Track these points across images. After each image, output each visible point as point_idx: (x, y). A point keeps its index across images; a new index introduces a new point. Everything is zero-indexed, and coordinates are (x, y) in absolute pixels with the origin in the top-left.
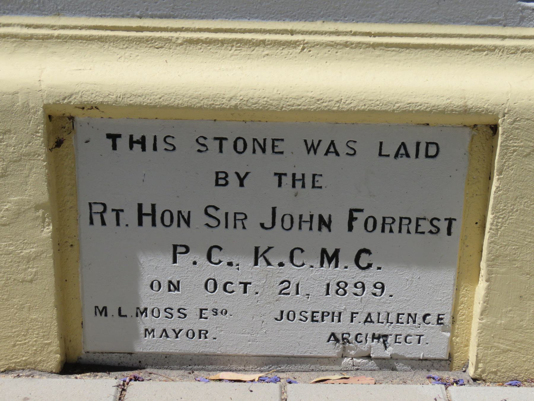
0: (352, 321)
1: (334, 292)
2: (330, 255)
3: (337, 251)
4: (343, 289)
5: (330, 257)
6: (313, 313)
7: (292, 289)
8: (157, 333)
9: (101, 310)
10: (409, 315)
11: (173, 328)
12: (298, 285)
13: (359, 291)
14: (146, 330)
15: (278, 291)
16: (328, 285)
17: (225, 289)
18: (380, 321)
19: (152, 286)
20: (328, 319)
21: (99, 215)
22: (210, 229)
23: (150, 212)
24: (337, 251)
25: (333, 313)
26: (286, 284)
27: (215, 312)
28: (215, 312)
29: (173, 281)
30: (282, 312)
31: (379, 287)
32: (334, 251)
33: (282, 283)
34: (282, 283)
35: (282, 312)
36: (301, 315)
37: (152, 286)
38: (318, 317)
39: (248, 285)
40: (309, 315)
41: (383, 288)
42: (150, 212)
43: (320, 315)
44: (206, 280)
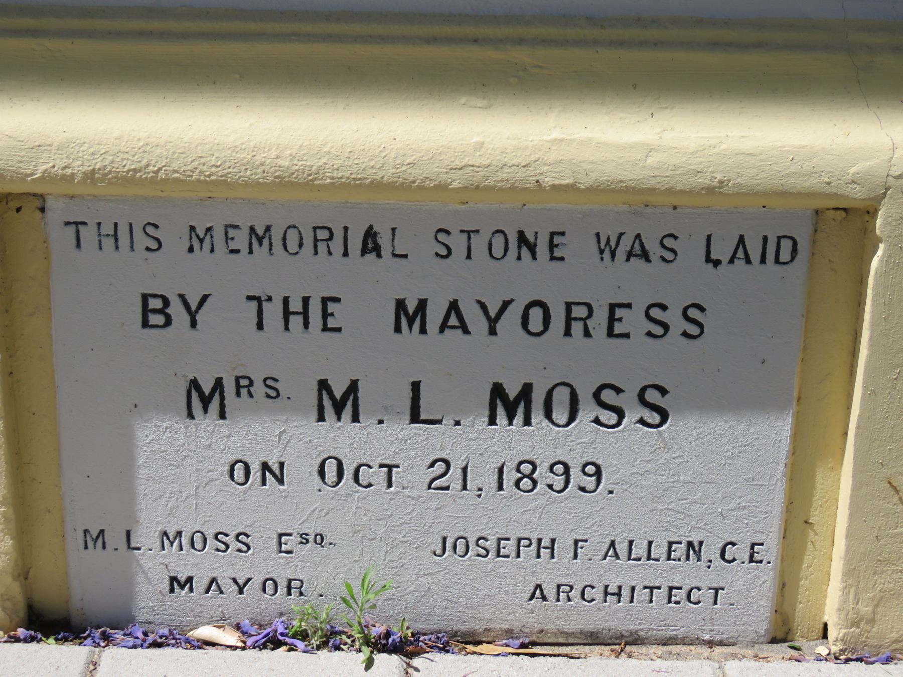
0: (576, 556)
1: (512, 483)
2: (338, 395)
3: (353, 387)
4: (530, 476)
5: (340, 401)
6: (499, 540)
7: (454, 477)
8: (200, 584)
9: (94, 537)
10: (690, 544)
11: (233, 576)
12: (465, 470)
13: (559, 482)
14: (173, 579)
15: (426, 486)
16: (501, 471)
17: (356, 479)
18: (653, 556)
19: (322, 473)
20: (528, 552)
21: (581, 324)
22: (692, 342)
23: (301, 310)
24: (353, 387)
25: (540, 541)
26: (440, 467)
27: (304, 539)
28: (304, 539)
29: (270, 463)
30: (444, 539)
31: (591, 473)
32: (347, 383)
33: (432, 465)
34: (432, 465)
35: (444, 539)
36: (478, 545)
37: (322, 473)
38: (509, 547)
39: (394, 470)
40: (491, 544)
41: (598, 474)
42: (301, 310)
43: (512, 543)
44: (319, 460)
